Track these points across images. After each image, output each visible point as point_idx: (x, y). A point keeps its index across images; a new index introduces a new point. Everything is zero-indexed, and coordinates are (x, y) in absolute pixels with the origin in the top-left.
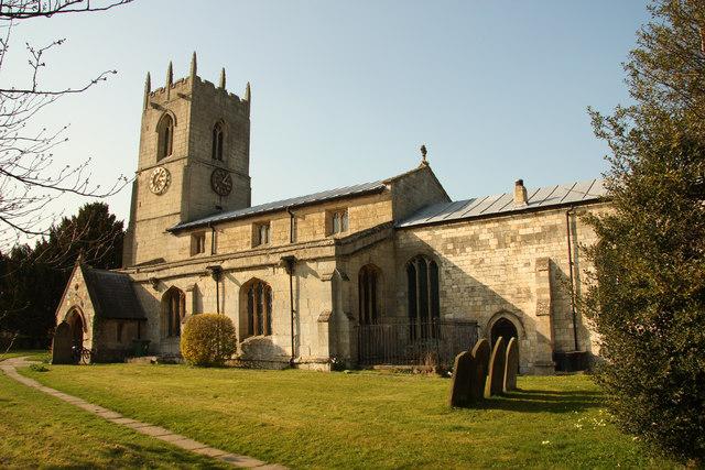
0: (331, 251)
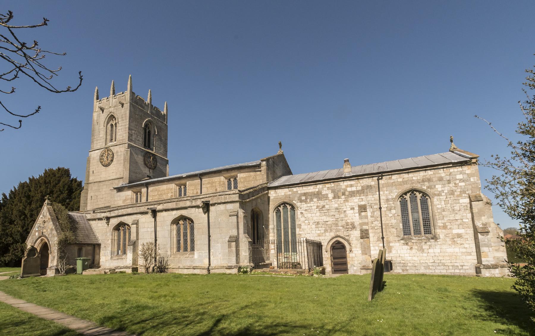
0: (236, 198)
